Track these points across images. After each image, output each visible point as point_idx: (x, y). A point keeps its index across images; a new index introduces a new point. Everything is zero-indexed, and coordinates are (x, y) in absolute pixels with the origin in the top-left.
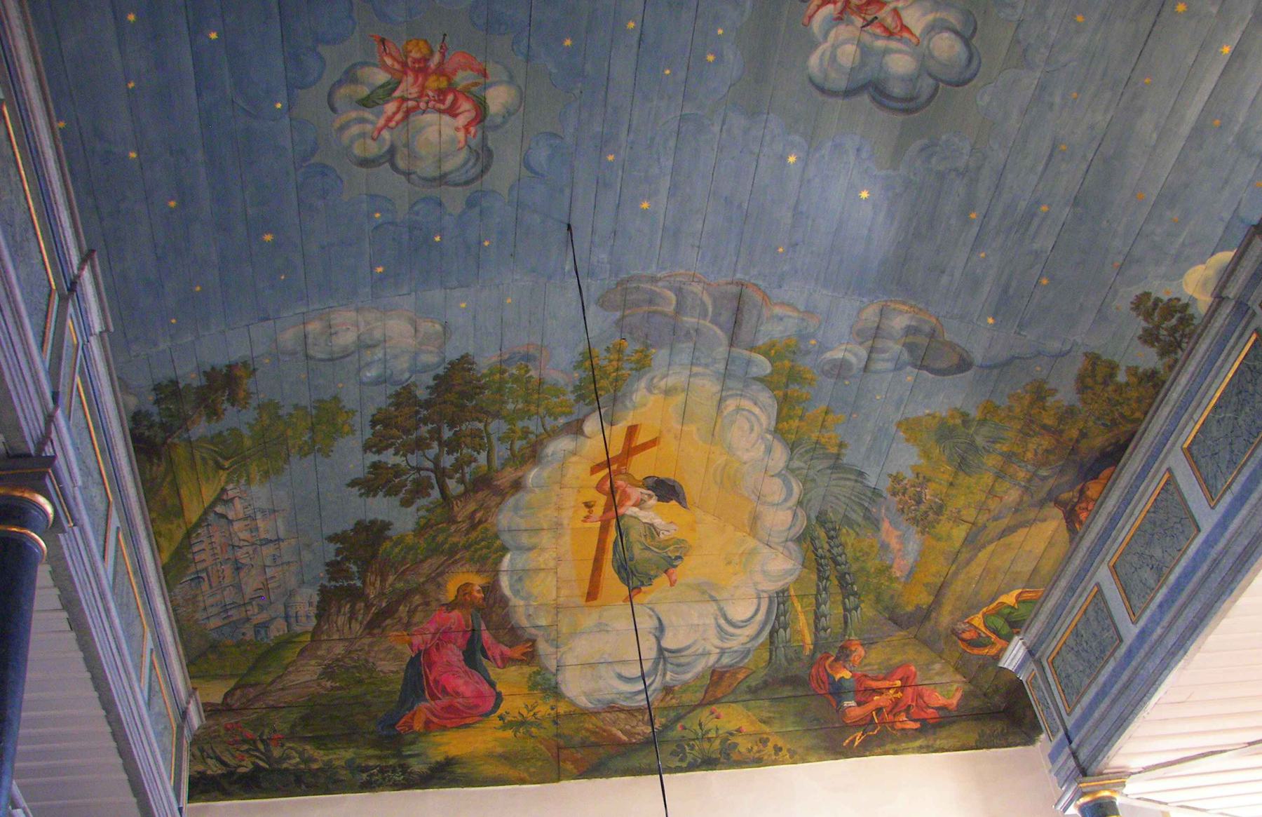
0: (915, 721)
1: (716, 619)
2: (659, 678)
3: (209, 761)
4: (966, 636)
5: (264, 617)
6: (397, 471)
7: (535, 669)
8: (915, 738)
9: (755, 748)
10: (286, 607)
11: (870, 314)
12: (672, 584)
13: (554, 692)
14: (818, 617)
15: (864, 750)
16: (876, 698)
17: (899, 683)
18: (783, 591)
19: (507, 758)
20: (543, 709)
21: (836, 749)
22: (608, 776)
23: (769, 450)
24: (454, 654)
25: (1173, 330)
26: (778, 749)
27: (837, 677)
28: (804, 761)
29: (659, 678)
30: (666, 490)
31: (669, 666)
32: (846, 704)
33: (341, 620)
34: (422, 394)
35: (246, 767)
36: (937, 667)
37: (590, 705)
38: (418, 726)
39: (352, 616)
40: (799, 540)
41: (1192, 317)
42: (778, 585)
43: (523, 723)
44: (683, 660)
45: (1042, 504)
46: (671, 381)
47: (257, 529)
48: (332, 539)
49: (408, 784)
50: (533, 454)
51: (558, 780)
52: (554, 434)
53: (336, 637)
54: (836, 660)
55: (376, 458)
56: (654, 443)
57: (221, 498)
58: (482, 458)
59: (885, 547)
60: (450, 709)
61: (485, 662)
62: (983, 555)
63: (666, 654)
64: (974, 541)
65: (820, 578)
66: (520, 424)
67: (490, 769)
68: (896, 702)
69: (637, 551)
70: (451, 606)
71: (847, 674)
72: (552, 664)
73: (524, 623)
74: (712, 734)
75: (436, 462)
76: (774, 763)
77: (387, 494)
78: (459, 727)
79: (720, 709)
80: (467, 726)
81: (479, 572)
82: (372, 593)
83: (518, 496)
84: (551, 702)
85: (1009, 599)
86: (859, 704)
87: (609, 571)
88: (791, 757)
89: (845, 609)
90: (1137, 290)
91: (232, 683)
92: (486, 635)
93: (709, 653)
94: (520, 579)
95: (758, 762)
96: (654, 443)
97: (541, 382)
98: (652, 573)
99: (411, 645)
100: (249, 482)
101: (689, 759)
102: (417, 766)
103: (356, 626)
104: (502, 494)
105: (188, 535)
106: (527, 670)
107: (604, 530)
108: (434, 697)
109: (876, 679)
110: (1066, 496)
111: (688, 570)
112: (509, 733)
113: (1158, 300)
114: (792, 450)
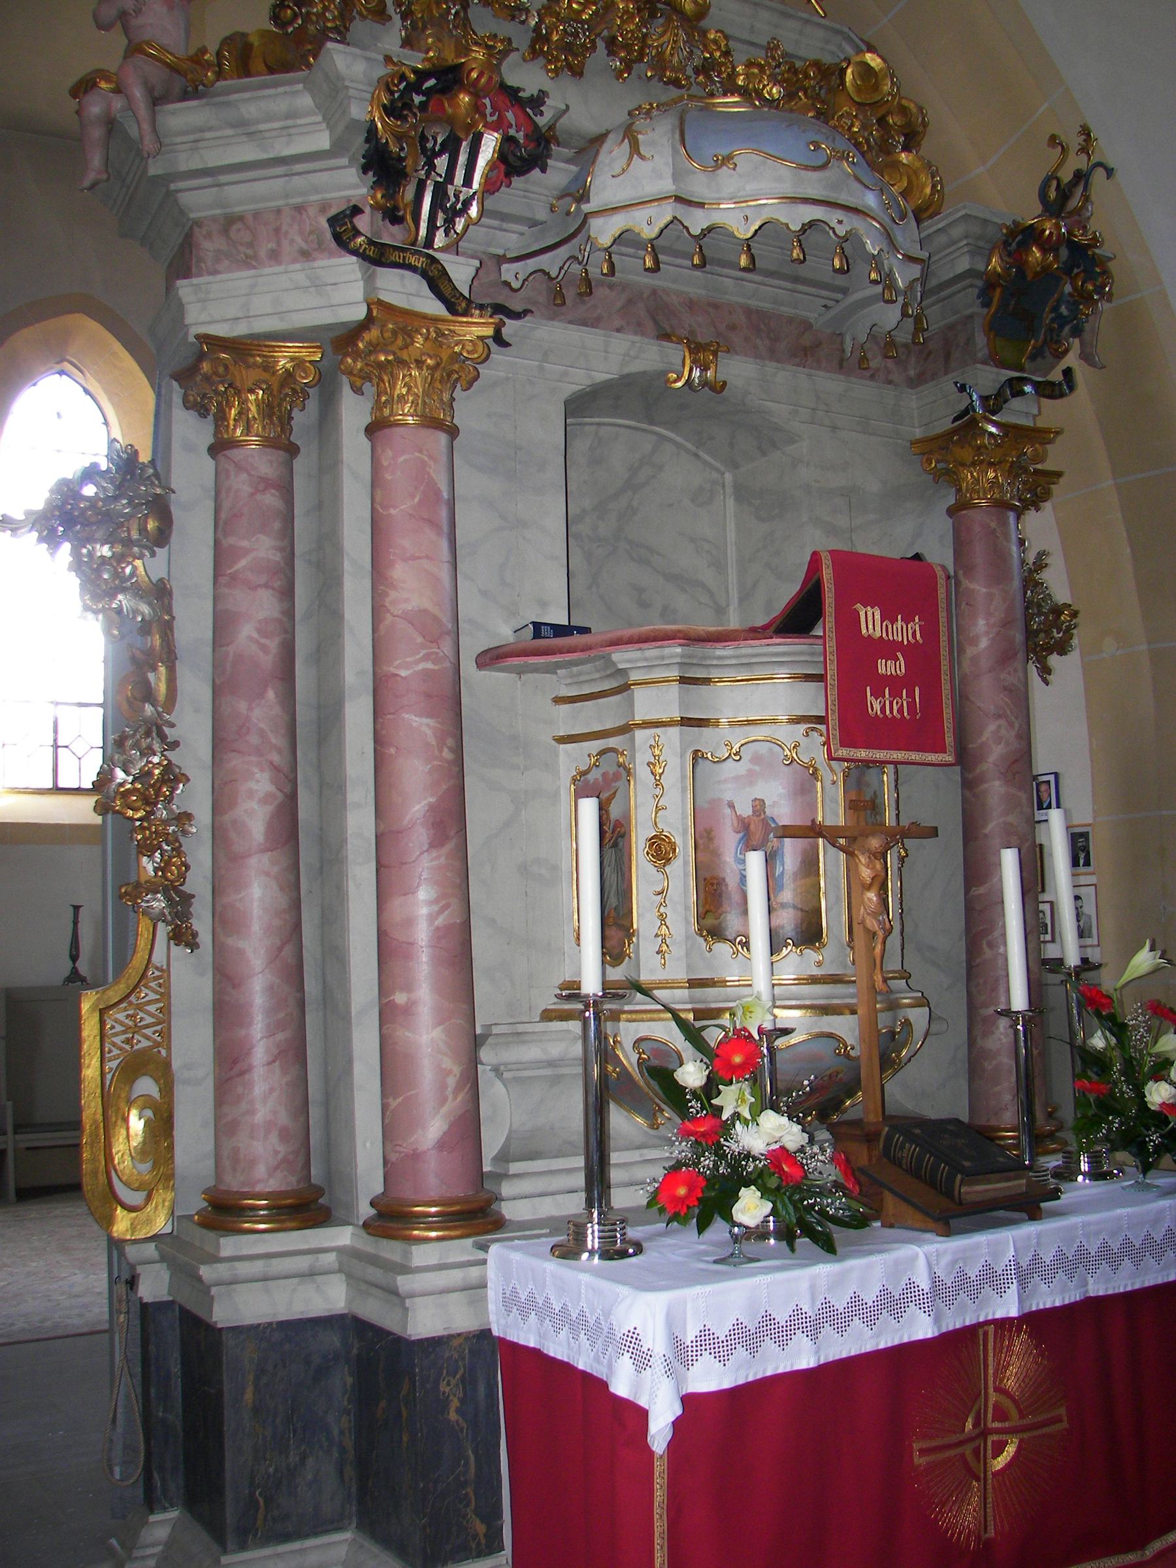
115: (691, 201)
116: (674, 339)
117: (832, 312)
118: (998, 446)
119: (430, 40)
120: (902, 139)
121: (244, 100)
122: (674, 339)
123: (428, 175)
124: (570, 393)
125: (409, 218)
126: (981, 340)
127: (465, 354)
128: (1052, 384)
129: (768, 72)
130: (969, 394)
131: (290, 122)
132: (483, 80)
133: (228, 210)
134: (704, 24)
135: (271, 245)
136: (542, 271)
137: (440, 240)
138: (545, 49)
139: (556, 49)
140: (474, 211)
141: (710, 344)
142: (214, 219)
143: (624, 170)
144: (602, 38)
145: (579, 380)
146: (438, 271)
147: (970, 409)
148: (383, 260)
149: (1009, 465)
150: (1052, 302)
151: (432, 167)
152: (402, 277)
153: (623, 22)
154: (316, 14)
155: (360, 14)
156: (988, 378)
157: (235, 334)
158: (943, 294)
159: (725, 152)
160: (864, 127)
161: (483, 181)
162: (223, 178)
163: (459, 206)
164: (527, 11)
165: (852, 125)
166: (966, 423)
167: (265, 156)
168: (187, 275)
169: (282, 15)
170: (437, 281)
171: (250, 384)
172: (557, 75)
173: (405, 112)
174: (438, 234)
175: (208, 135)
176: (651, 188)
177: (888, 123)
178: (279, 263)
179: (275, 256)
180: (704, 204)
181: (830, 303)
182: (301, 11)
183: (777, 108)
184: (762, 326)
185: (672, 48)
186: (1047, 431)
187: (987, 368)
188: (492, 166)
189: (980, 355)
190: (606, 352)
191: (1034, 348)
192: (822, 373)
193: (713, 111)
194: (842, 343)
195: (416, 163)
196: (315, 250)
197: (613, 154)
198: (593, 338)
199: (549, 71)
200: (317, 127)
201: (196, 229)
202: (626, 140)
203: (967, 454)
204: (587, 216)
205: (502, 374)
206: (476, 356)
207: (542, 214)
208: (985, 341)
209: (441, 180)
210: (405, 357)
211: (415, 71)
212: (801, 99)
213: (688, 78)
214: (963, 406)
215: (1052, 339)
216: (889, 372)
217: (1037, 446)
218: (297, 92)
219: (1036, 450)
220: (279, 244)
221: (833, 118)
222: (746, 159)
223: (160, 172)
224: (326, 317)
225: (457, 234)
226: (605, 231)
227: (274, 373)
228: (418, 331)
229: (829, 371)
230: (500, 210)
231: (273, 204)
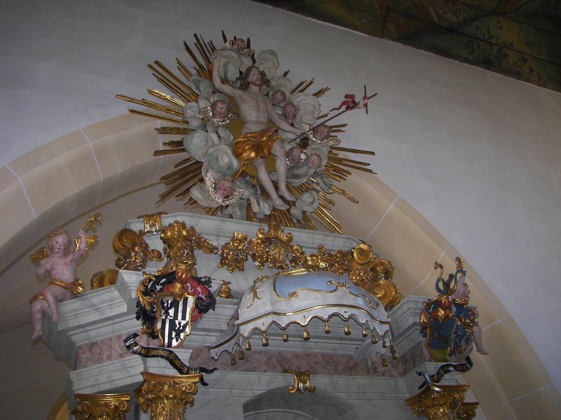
22: (418, 46)
51: (381, 36)
95: (517, 75)
115: (280, 313)
116: (289, 371)
117: (359, 350)
118: (442, 396)
119: (172, 264)
120: (383, 275)
121: (91, 297)
122: (289, 371)
123: (166, 317)
124: (244, 402)
125: (160, 336)
126: (426, 351)
127: (187, 391)
128: (462, 365)
129: (320, 258)
130: (423, 375)
131: (111, 303)
132: (183, 276)
133: (91, 341)
134: (291, 244)
135: (108, 353)
136: (226, 351)
137: (174, 343)
138: (227, 262)
139: (231, 261)
140: (187, 330)
141: (306, 372)
142: (86, 345)
143: (251, 304)
144: (250, 255)
145: (249, 395)
146: (173, 356)
147: (425, 382)
148: (149, 354)
149: (449, 404)
150: (453, 331)
151: (167, 314)
152: (158, 361)
153: (257, 248)
154: (132, 261)
155: (150, 259)
156: (431, 368)
157: (93, 392)
158: (407, 335)
159: (293, 291)
160: (364, 273)
161: (190, 317)
162: (88, 328)
163: (181, 328)
164: (217, 249)
165: (360, 273)
166: (426, 389)
167: (103, 317)
168: (75, 368)
169: (120, 263)
170: (174, 361)
171: (99, 414)
172: (233, 271)
173: (151, 293)
174: (173, 341)
175: (80, 312)
176: (263, 311)
177: (376, 270)
178: (111, 360)
179: (109, 357)
180: (286, 313)
181: (358, 346)
182: (127, 261)
183: (327, 270)
184: (330, 360)
185: (279, 255)
186: (464, 386)
187: (431, 363)
188: (193, 310)
189: (427, 358)
190: (260, 381)
191: (450, 350)
192: (359, 377)
193: (292, 275)
194: (367, 362)
195: (161, 313)
196: (125, 353)
197: (248, 298)
198: (253, 376)
199: (229, 270)
200: (121, 303)
201: (79, 350)
202: (252, 292)
203: (429, 402)
204: (239, 325)
205: (214, 397)
206: (192, 391)
207: (224, 327)
208: (428, 352)
209: (172, 318)
210: (161, 395)
211: (155, 276)
212: (336, 266)
213: (287, 265)
214: (422, 382)
215: (457, 345)
216: (391, 371)
217: (460, 393)
218: (113, 290)
219: (460, 395)
220: (111, 353)
221: (352, 271)
222: (302, 293)
223: (62, 329)
224: (129, 381)
225: (182, 340)
226: (246, 330)
227: (110, 408)
228: (165, 383)
229: (363, 376)
230: (205, 327)
231: (109, 336)
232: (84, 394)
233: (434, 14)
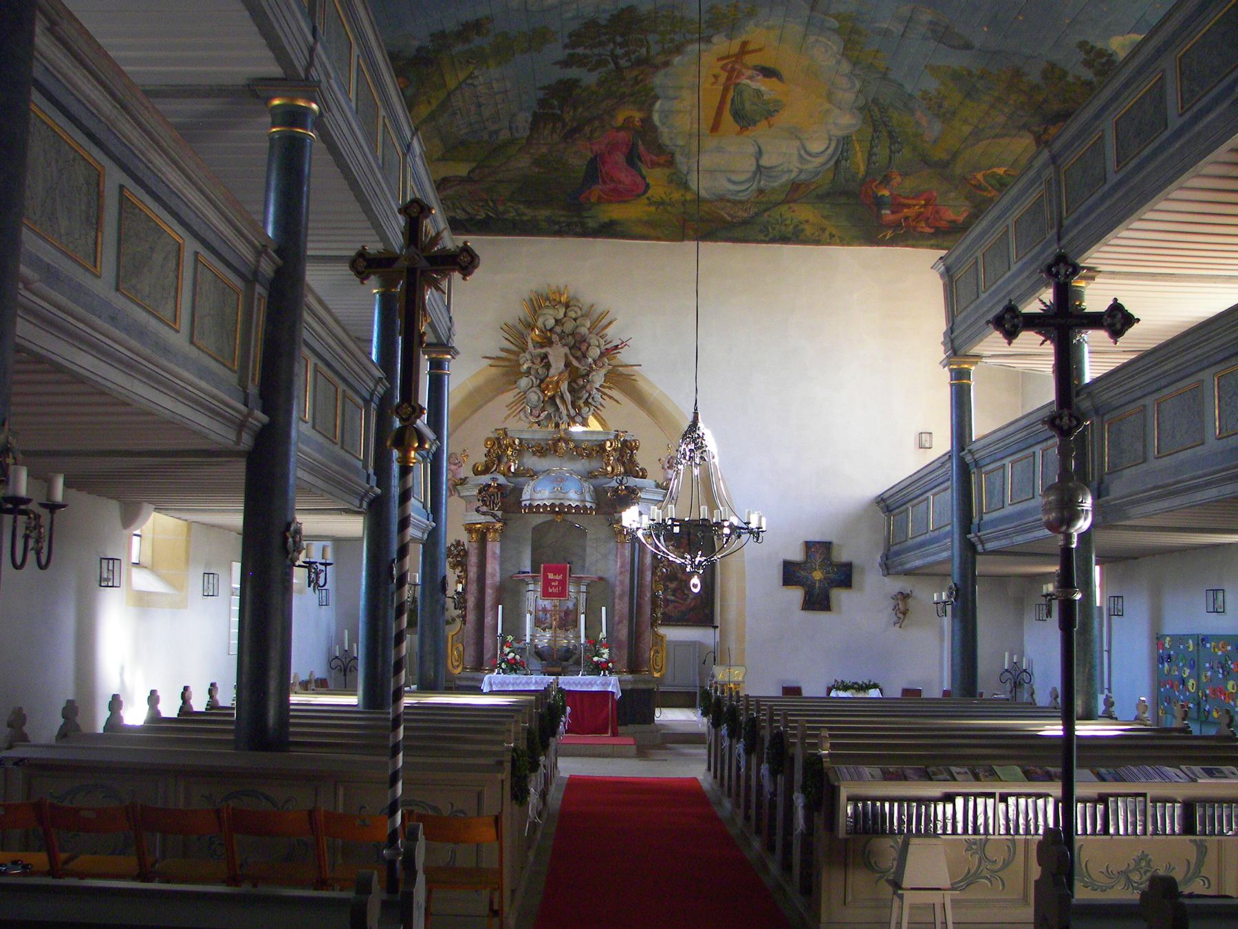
0: (931, 228)
1: (798, 151)
2: (756, 183)
3: (458, 210)
4: (973, 182)
5: (495, 127)
6: (586, 56)
7: (673, 171)
8: (929, 239)
9: (817, 233)
10: (510, 122)
11: (905, 10)
12: (770, 126)
13: (685, 186)
14: (870, 155)
15: (892, 242)
16: (905, 210)
17: (923, 202)
18: (847, 137)
19: (650, 224)
20: (676, 196)
21: (872, 239)
22: (716, 240)
23: (839, 63)
24: (620, 158)
25: (1103, 65)
26: (832, 236)
27: (879, 194)
28: (849, 245)
29: (756, 183)
30: (768, 72)
31: (763, 176)
32: (883, 212)
33: (546, 132)
34: (603, 22)
35: (482, 215)
36: (952, 195)
37: (708, 196)
38: (593, 200)
39: (553, 131)
40: (861, 109)
41: (1114, 62)
42: (845, 133)
43: (662, 203)
44: (775, 174)
45: (1020, 128)
46: (771, 23)
47: (493, 88)
48: (541, 89)
49: (585, 234)
50: (679, 49)
51: (682, 240)
52: (692, 41)
53: (542, 142)
54: (881, 183)
55: (572, 51)
56: (760, 50)
57: (471, 76)
58: (644, 51)
59: (918, 124)
60: (615, 190)
61: (639, 163)
62: (983, 144)
63: (762, 169)
64: (976, 134)
65: (875, 131)
66: (668, 37)
67: (639, 230)
68: (919, 215)
69: (748, 105)
70: (620, 129)
71: (886, 193)
72: (684, 169)
73: (668, 142)
74: (788, 222)
75: (612, 54)
76: (829, 244)
77: (579, 66)
78: (620, 202)
79: (795, 206)
80: (624, 202)
81: (639, 110)
82: (567, 117)
83: (666, 69)
84: (682, 192)
85: (1001, 171)
86: (893, 212)
87: (727, 116)
88: (841, 241)
89: (891, 151)
90: (1081, 39)
91: (474, 165)
92: (641, 148)
93: (791, 171)
94: (666, 117)
95: (817, 242)
96: (760, 50)
97: (682, 18)
98: (757, 119)
99: (592, 151)
100: (488, 67)
101: (771, 236)
102: (591, 224)
103: (555, 137)
104: (657, 68)
105: (449, 95)
106: (667, 171)
107: (726, 89)
108: (604, 182)
109: (907, 198)
110: (1036, 129)
111: (784, 118)
112: (653, 209)
113: (1093, 47)
114: (854, 65)
232: (946, 298)
233: (726, 215)
